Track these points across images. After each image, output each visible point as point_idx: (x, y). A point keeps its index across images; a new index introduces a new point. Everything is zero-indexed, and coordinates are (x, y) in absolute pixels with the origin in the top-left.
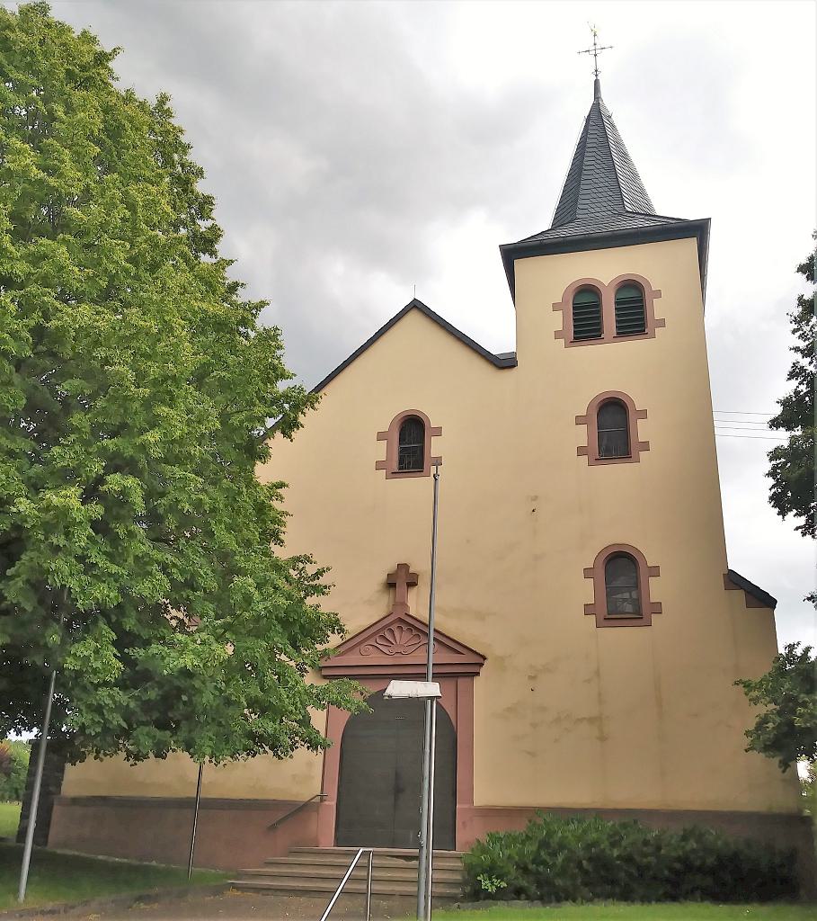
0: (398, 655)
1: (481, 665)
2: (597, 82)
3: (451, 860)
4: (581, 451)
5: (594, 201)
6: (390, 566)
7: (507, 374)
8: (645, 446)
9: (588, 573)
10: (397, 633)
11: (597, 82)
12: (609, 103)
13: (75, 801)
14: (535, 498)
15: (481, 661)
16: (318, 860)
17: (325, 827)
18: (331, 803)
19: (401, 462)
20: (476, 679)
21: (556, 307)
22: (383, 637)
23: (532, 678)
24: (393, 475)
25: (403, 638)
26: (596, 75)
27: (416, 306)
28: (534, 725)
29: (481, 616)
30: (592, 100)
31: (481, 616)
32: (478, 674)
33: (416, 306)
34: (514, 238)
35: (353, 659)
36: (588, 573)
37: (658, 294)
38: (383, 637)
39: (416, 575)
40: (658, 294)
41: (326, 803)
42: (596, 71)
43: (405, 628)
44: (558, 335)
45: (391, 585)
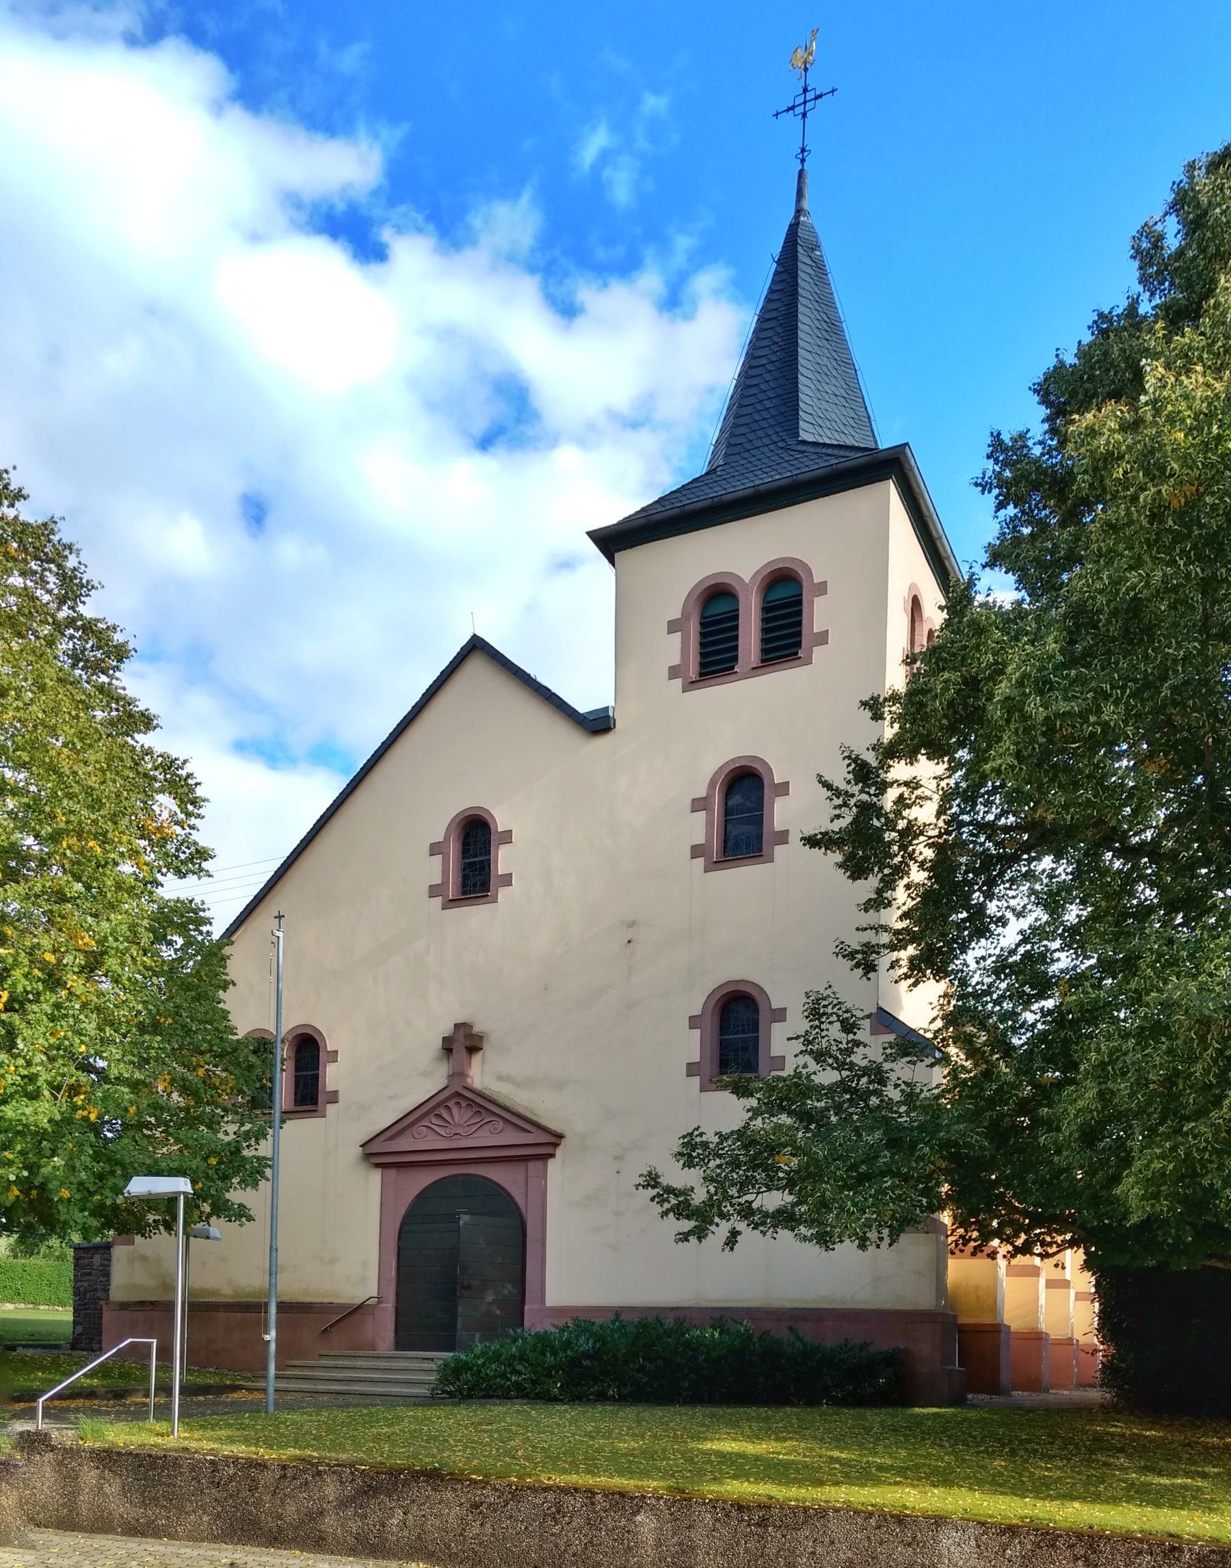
0: (458, 1137)
1: (556, 1145)
2: (801, 174)
3: (415, 1361)
4: (696, 851)
5: (755, 426)
6: (446, 1028)
7: (603, 742)
8: (507, 880)
9: (694, 1022)
10: (455, 1110)
11: (801, 174)
12: (818, 220)
13: (124, 1306)
14: (632, 924)
15: (552, 1140)
16: (372, 1364)
17: (384, 1328)
18: (390, 1305)
19: (464, 885)
20: (551, 1163)
21: (673, 627)
22: (439, 1116)
23: (617, 1158)
24: (714, 865)
25: (460, 1115)
26: (803, 161)
27: (476, 646)
28: (618, 1214)
29: (559, 1086)
30: (792, 213)
31: (559, 1086)
32: (552, 1156)
33: (476, 646)
34: (613, 513)
35: (404, 1144)
36: (694, 1022)
37: (822, 588)
38: (439, 1116)
39: (480, 1038)
40: (822, 588)
41: (384, 1305)
42: (803, 150)
43: (464, 1104)
44: (674, 672)
45: (448, 1046)
